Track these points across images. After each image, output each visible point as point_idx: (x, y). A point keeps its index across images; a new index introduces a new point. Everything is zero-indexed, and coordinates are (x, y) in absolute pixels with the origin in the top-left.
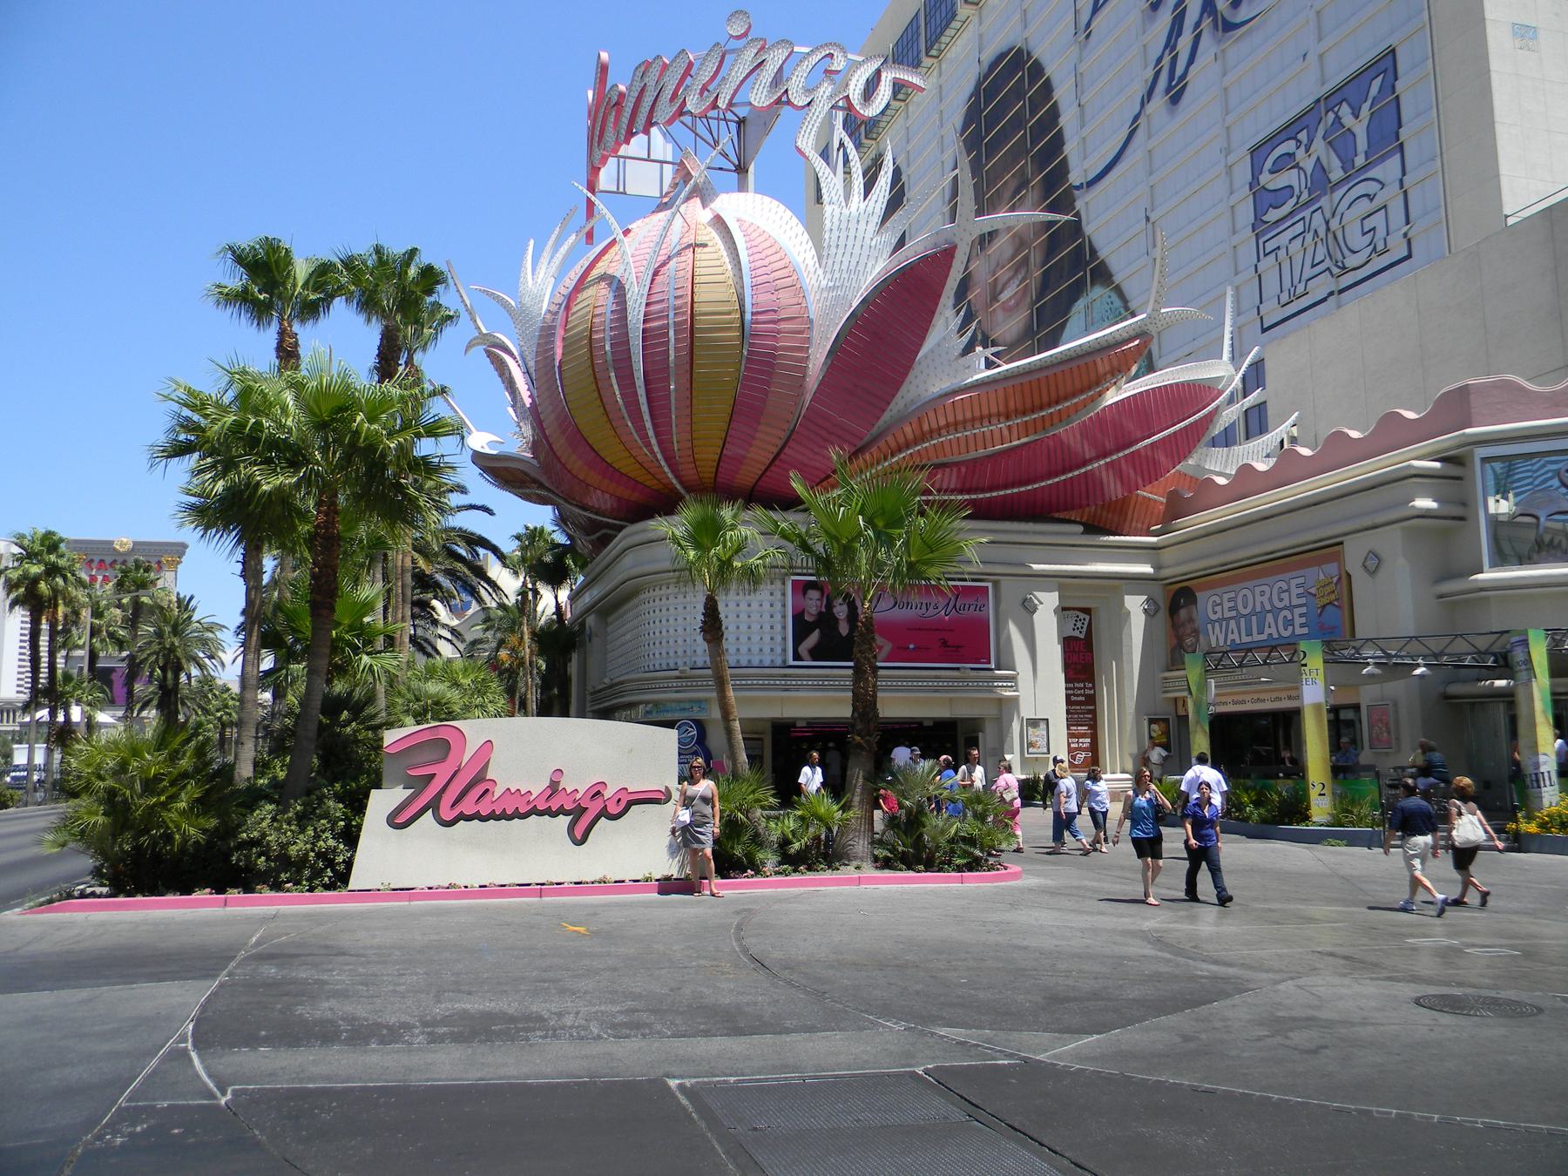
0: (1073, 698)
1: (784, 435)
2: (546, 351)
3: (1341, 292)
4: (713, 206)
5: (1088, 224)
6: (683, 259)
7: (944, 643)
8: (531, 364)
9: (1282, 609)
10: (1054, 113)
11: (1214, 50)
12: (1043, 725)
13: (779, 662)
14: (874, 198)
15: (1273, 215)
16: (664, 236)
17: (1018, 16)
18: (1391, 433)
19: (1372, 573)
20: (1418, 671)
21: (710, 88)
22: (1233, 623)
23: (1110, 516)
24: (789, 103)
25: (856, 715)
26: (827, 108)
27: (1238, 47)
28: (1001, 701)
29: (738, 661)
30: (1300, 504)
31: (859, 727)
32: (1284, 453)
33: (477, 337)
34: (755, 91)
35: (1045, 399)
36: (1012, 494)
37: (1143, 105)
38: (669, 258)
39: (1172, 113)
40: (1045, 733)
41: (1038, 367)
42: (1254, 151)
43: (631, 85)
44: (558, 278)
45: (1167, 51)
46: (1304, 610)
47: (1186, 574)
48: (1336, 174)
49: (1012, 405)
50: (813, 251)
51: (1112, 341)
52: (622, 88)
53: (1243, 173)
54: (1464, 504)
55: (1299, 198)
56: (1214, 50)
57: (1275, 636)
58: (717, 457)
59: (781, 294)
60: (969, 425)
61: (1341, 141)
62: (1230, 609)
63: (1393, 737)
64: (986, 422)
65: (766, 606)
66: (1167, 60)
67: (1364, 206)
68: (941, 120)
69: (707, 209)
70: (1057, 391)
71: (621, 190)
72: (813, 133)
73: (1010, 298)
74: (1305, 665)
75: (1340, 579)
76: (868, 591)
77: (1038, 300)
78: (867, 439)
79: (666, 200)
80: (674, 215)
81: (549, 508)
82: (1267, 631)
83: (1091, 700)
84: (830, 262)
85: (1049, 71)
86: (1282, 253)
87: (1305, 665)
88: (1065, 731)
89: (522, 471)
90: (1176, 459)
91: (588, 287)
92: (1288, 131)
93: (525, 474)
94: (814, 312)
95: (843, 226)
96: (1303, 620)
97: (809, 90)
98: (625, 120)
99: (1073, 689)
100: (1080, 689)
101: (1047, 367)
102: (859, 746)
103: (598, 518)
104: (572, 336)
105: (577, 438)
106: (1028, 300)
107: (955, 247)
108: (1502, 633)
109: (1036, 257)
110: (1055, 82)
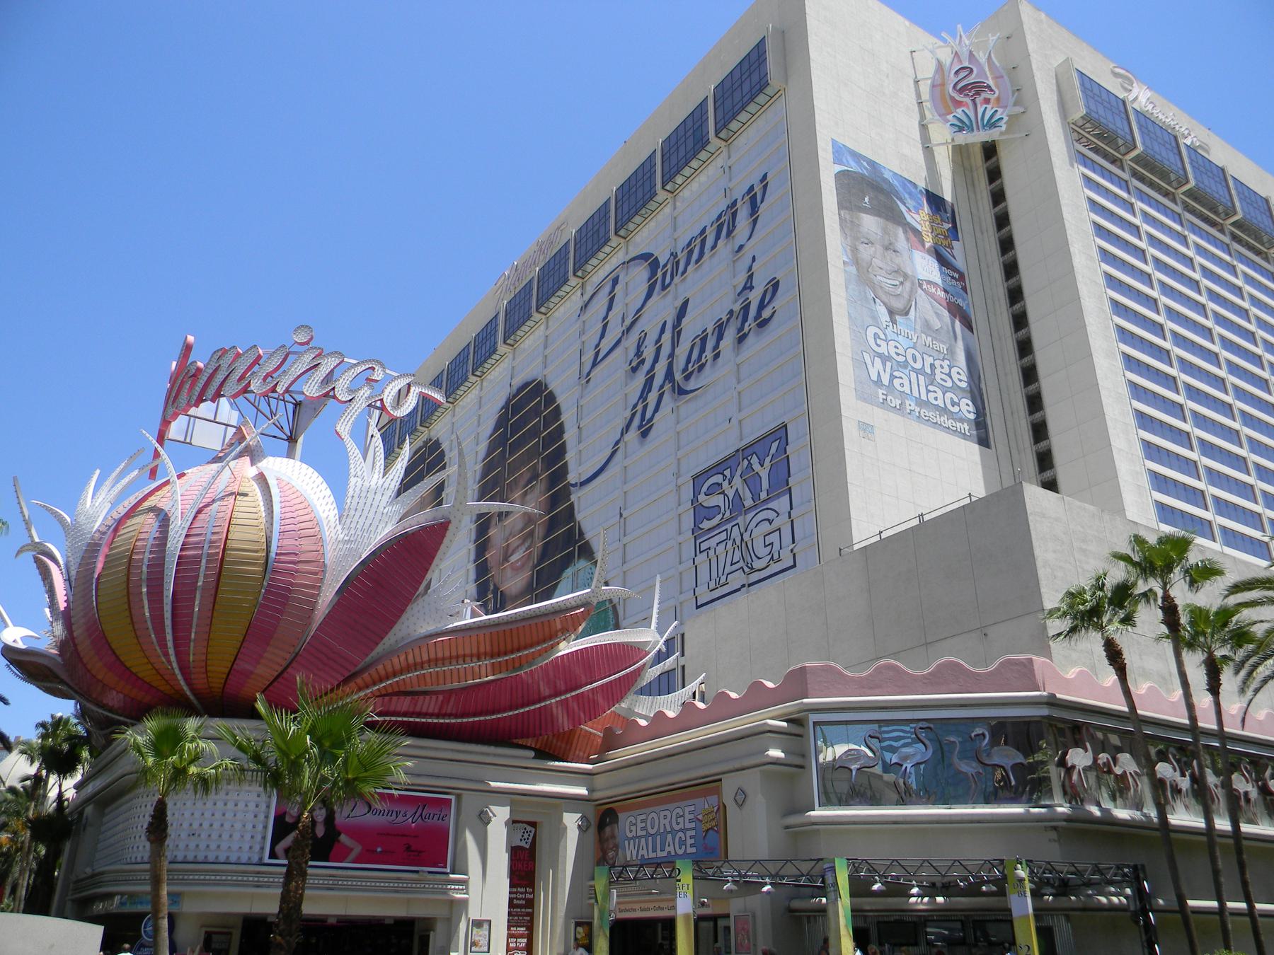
0: (516, 902)
1: (289, 657)
2: (88, 564)
3: (750, 585)
4: (260, 465)
5: (579, 512)
6: (225, 503)
7: (408, 848)
8: (73, 573)
9: (678, 831)
10: (560, 430)
11: (672, 405)
12: (486, 926)
13: (255, 859)
14: (391, 477)
15: (706, 525)
16: (211, 483)
17: (540, 359)
18: (757, 697)
19: (740, 805)
20: (765, 889)
21: (274, 375)
22: (643, 840)
23: (563, 746)
24: (334, 397)
25: (281, 916)
26: (364, 406)
27: (687, 406)
28: (452, 903)
29: (206, 857)
30: (693, 747)
31: (281, 927)
32: (687, 707)
33: (29, 545)
34: (308, 385)
35: (509, 647)
36: (480, 721)
37: (622, 434)
38: (213, 501)
39: (642, 444)
40: (487, 933)
41: (505, 621)
42: (695, 478)
43: (208, 364)
44: (114, 505)
45: (641, 401)
46: (693, 833)
47: (611, 797)
48: (748, 502)
49: (482, 650)
50: (336, 511)
51: (563, 607)
52: (200, 365)
53: (688, 492)
54: (803, 756)
55: (723, 515)
56: (672, 405)
57: (673, 853)
58: (227, 671)
59: (303, 541)
60: (447, 662)
61: (751, 480)
62: (642, 829)
63: (752, 944)
64: (461, 661)
65: (252, 806)
66: (640, 407)
67: (766, 527)
68: (479, 422)
69: (254, 467)
70: (478, 648)
71: (188, 441)
72: (351, 422)
73: (518, 560)
74: (679, 881)
75: (718, 809)
76: (309, 803)
77: (538, 564)
78: (359, 667)
79: (221, 455)
80: (223, 468)
81: (72, 702)
82: (667, 849)
83: (531, 903)
84: (349, 521)
85: (559, 400)
86: (711, 552)
87: (679, 881)
88: (506, 932)
89: (46, 667)
90: (611, 703)
91: (138, 515)
92: (718, 468)
93: (50, 670)
94: (329, 557)
95: (363, 495)
96: (693, 841)
97: (351, 391)
98: (198, 389)
99: (516, 893)
100: (521, 893)
101: (512, 622)
102: (279, 946)
103: (114, 716)
104: (114, 555)
105: (100, 639)
106: (531, 564)
107: (449, 522)
108: (819, 860)
109: (539, 532)
110: (563, 408)
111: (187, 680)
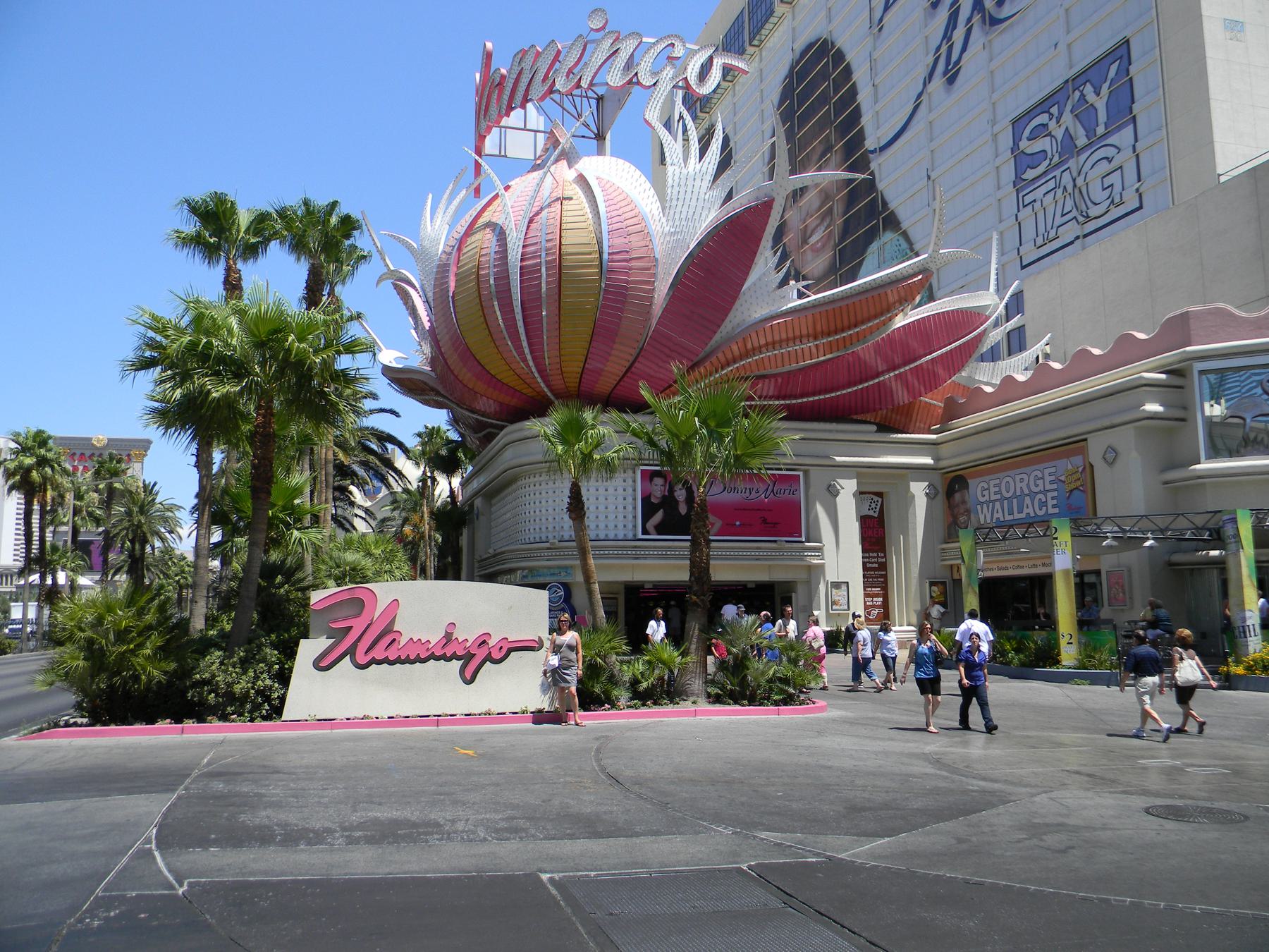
0: (869, 565)
1: (634, 353)
2: (442, 284)
3: (1085, 236)
4: (577, 166)
5: (880, 181)
6: (553, 209)
7: (764, 521)
8: (430, 295)
9: (1037, 493)
10: (853, 92)
11: (982, 40)
12: (844, 587)
13: (630, 536)
14: (708, 160)
15: (1030, 174)
16: (537, 191)
17: (824, 13)
18: (1126, 350)
19: (1111, 464)
20: (1148, 544)
21: (575, 71)
22: (998, 504)
23: (898, 417)
24: (638, 83)
25: (693, 579)
26: (669, 88)
27: (1002, 38)
28: (810, 568)
29: (597, 535)
30: (1052, 408)
31: (695, 588)
32: (1039, 367)
33: (386, 273)
34: (611, 74)
35: (846, 323)
36: (819, 400)
37: (925, 85)
38: (542, 209)
39: (948, 91)
40: (845, 593)
41: (840, 297)
42: (1015, 123)
43: (511, 69)
44: (452, 225)
45: (945, 42)
46: (1055, 494)
47: (959, 465)
48: (1082, 141)
49: (819, 328)
50: (658, 204)
51: (900, 276)
52: (504, 71)
53: (1006, 140)
54: (1185, 408)
55: (1051, 160)
56: (982, 40)
57: (1032, 515)
58: (580, 370)
59: (632, 238)
60: (784, 344)
61: (1085, 114)
62: (996, 493)
63: (1128, 596)
64: (798, 342)
65: (620, 490)
66: (944, 49)
67: (1104, 167)
68: (762, 97)
69: (573, 170)
70: (856, 316)
71: (503, 154)
72: (658, 107)
73: (818, 242)
74: (1056, 538)
75: (1084, 468)
76: (703, 478)
77: (840, 243)
78: (701, 355)
79: (539, 162)
80: (545, 174)
81: (444, 412)
82: (1026, 510)
83: (883, 567)
84: (672, 212)
85: (849, 58)
86: (1037, 205)
87: (1056, 538)
88: (862, 592)
89: (422, 381)
90: (952, 371)
91: (476, 233)
92: (1043, 106)
93: (425, 383)
94: (658, 252)
95: (682, 183)
96: (1055, 502)
97: (654, 73)
98: (506, 97)
99: (868, 558)
100: (874, 557)
101: (847, 297)
102: (695, 604)
103: (484, 419)
104: (463, 272)
105: (467, 355)
106: (832, 243)
107: (773, 200)
108: (1216, 512)
109: (838, 208)
110: (854, 67)
111: (548, 386)
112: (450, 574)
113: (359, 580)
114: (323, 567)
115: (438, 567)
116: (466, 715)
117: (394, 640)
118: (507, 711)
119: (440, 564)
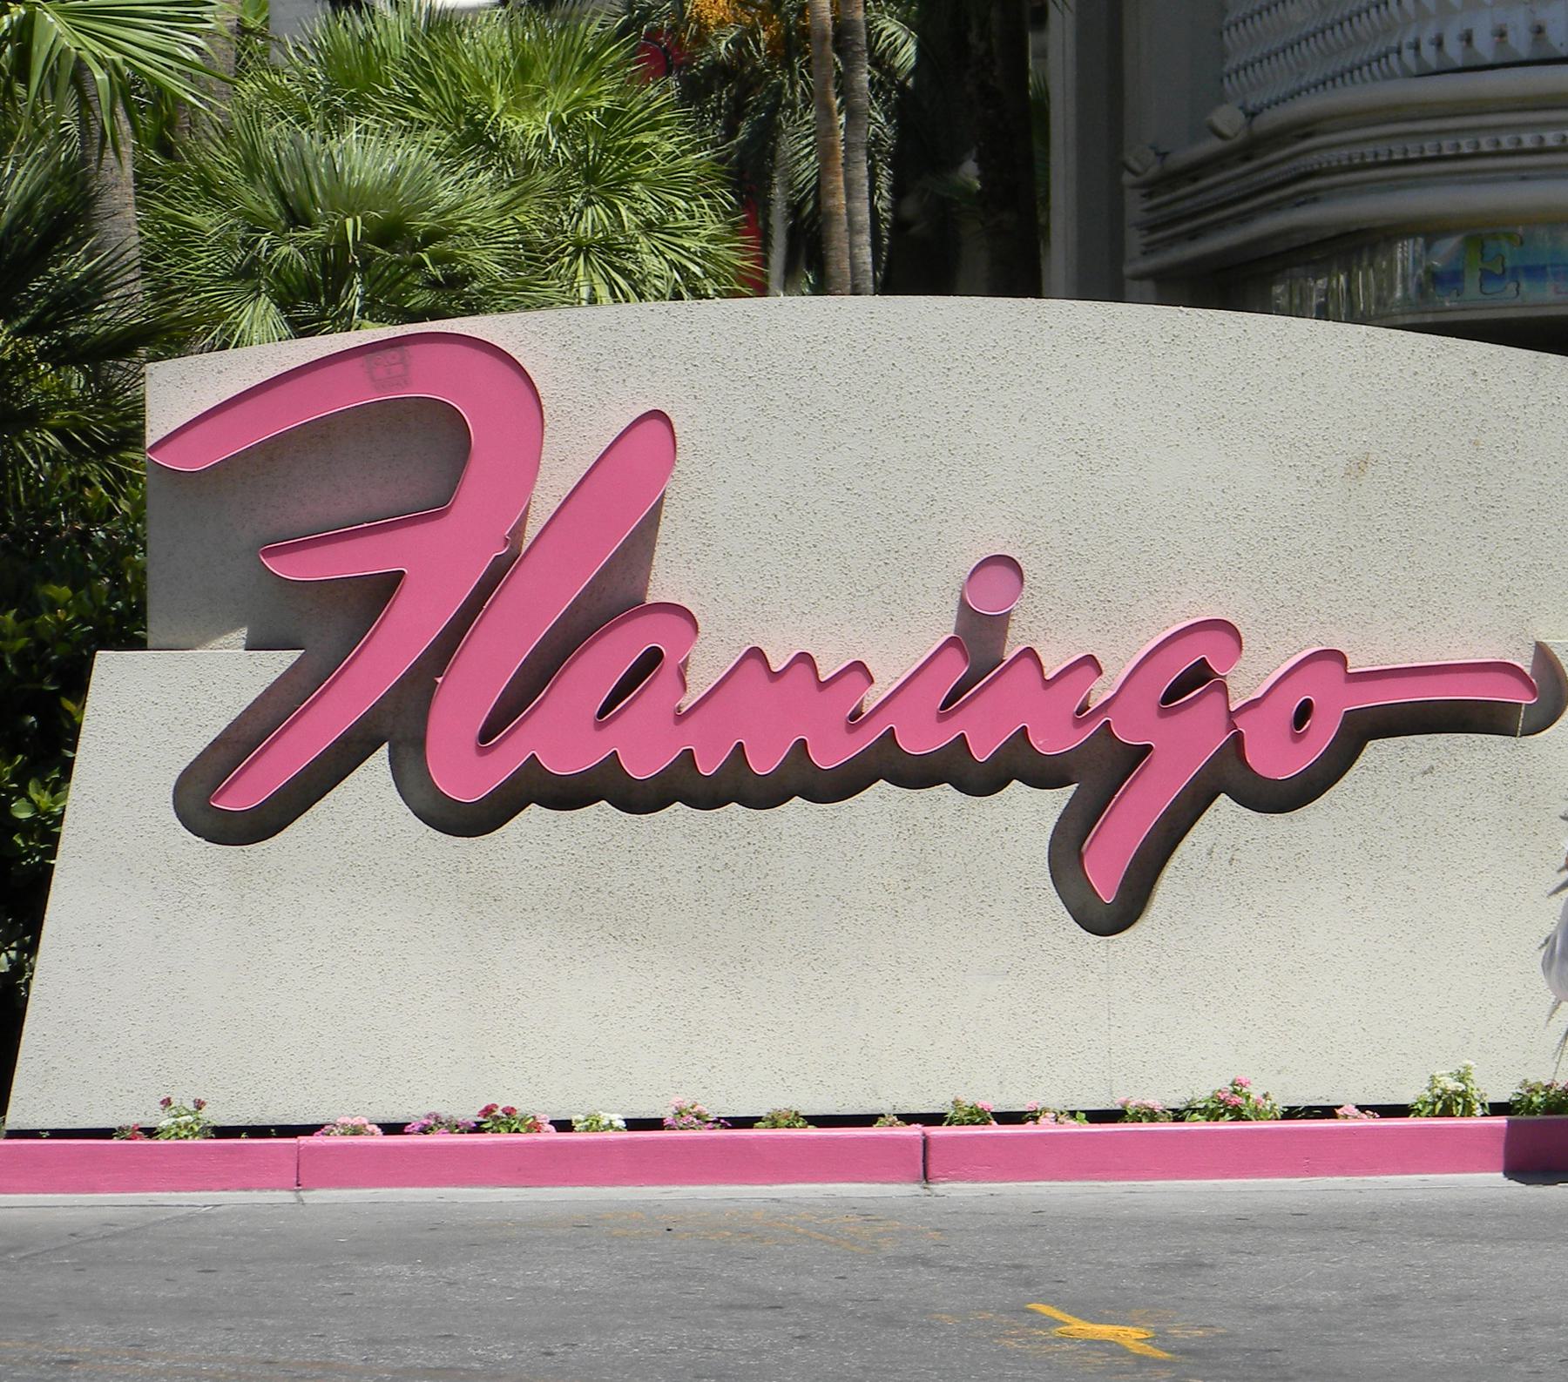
112: (976, 256)
113: (422, 298)
114: (206, 221)
115: (899, 226)
116: (1095, 1116)
117: (652, 659)
118: (1347, 1095)
119: (910, 208)
